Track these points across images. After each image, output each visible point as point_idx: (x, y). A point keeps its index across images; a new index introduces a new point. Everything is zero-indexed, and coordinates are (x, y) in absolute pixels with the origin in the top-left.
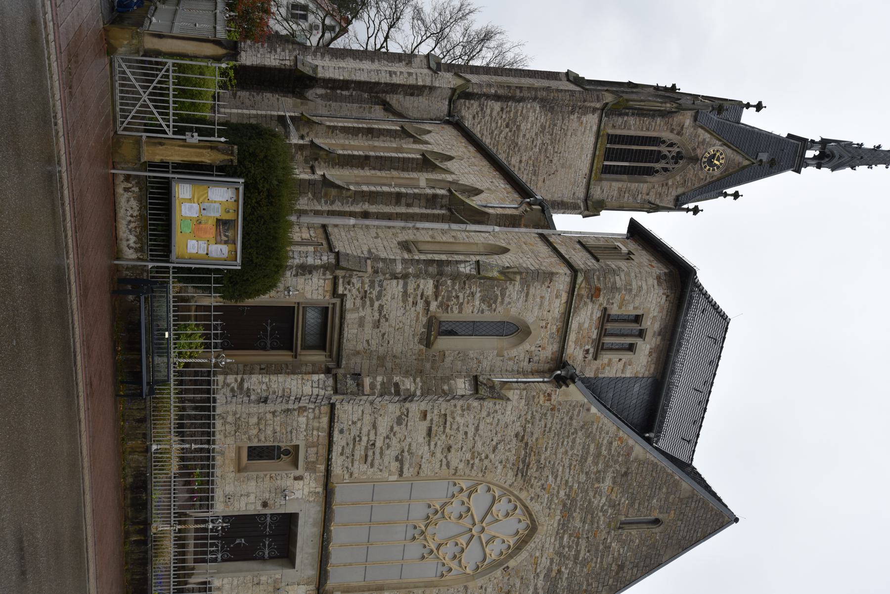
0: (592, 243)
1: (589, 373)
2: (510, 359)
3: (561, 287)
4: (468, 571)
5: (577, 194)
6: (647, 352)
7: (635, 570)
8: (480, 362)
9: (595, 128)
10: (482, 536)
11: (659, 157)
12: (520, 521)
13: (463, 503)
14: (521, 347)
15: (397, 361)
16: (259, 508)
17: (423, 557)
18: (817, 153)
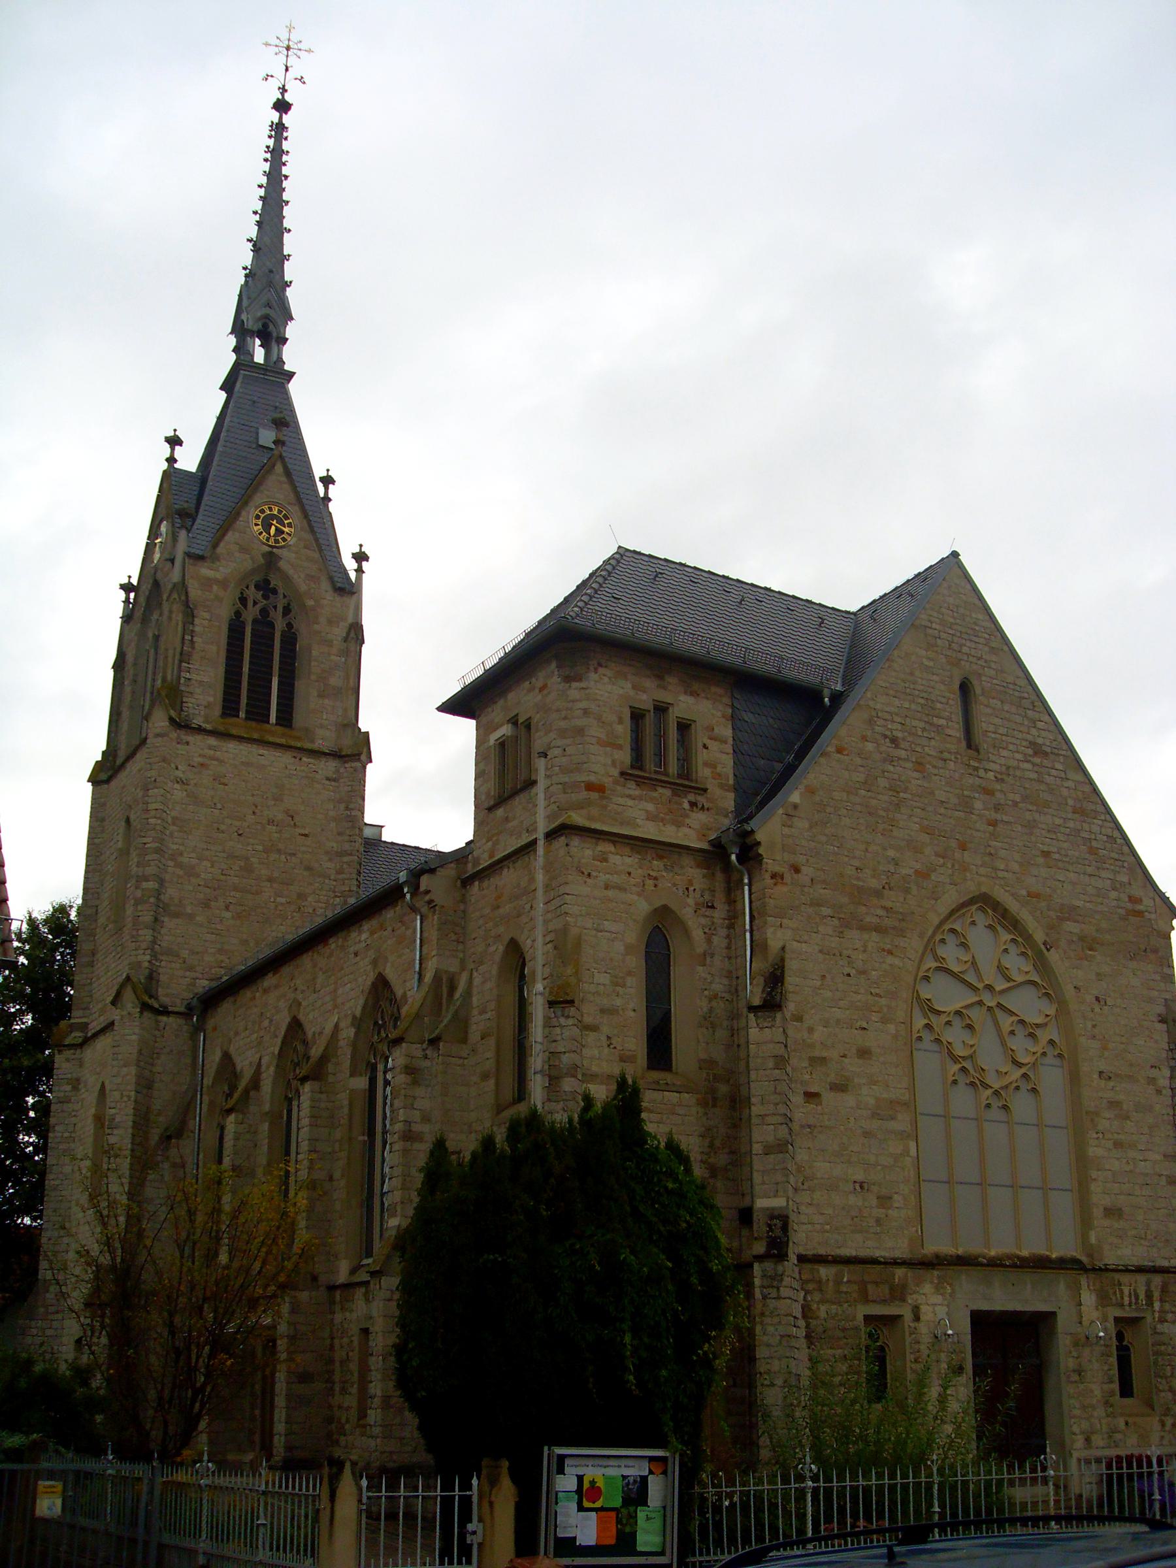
0: (491, 786)
1: (729, 801)
3: (588, 852)
4: (1052, 1011)
5: (331, 775)
6: (690, 700)
7: (1040, 725)
8: (715, 996)
9: (212, 741)
10: (998, 988)
11: (264, 622)
12: (973, 923)
13: (948, 1023)
15: (717, 1143)
17: (1034, 1090)
18: (258, 342)
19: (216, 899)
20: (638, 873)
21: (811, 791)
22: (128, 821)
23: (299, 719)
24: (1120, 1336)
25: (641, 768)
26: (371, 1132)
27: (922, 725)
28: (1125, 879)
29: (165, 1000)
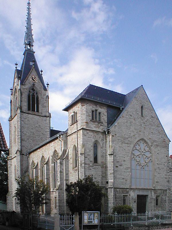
2: (103, 145)
3: (85, 132)
6: (101, 109)
8: (103, 153)
9: (27, 114)
14: (100, 143)
15: (104, 173)
16: (135, 203)
19: (29, 138)
20: (93, 135)
21: (118, 123)
22: (15, 127)
23: (40, 111)
24: (157, 198)
25: (93, 120)
26: (55, 172)
27: (135, 113)
28: (163, 136)
29: (23, 153)
